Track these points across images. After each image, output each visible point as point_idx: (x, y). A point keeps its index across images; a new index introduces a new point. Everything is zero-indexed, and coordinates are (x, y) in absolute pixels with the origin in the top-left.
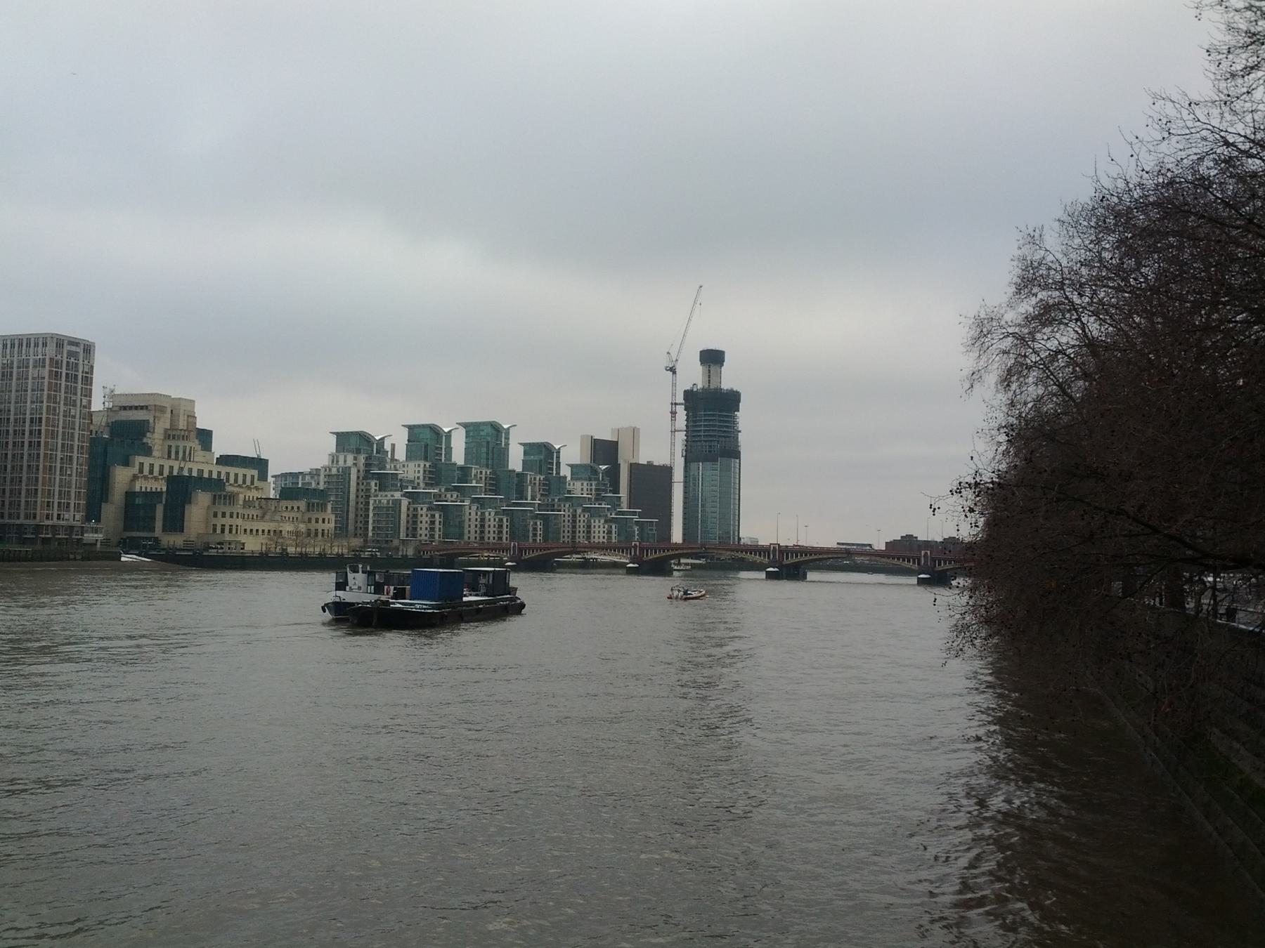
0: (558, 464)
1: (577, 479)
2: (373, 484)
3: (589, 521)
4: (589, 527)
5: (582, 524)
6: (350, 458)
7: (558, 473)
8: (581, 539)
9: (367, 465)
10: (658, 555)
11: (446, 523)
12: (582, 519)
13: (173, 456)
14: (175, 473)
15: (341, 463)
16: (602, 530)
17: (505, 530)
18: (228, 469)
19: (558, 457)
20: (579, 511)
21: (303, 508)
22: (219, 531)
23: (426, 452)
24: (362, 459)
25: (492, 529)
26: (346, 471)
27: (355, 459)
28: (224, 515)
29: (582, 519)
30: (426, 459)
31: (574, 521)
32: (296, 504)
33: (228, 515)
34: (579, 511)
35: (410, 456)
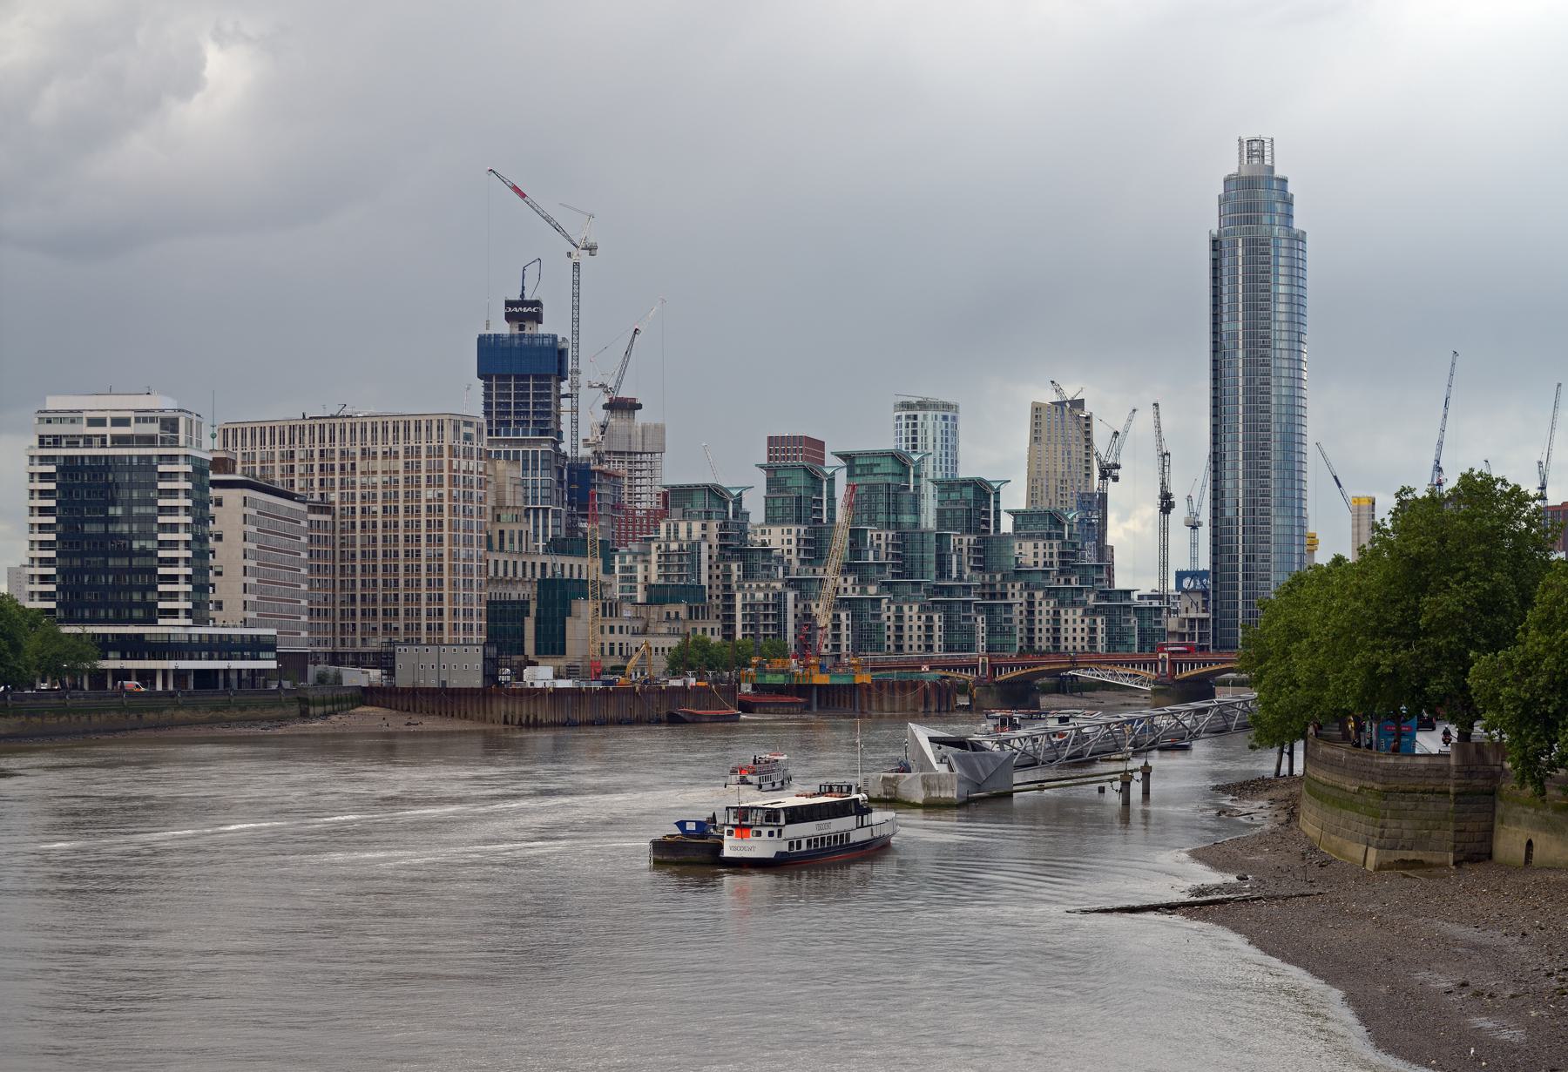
0: (997, 512)
1: (1030, 537)
2: (734, 567)
3: (1057, 613)
4: (1057, 621)
5: (1044, 617)
6: (696, 527)
7: (997, 529)
8: (1288, 531)
9: (722, 537)
10: (1196, 671)
11: (948, 627)
12: (1044, 608)
13: (496, 546)
14: (549, 575)
15: (683, 534)
16: (1079, 626)
17: (937, 633)
18: (560, 560)
19: (997, 502)
20: (1039, 595)
21: (683, 614)
22: (607, 652)
23: (799, 508)
24: (714, 528)
25: (1044, 626)
26: (694, 549)
27: (704, 527)
28: (612, 630)
29: (1045, 608)
30: (799, 521)
31: (1031, 613)
32: (671, 608)
33: (617, 630)
34: (1039, 595)
35: (771, 519)
